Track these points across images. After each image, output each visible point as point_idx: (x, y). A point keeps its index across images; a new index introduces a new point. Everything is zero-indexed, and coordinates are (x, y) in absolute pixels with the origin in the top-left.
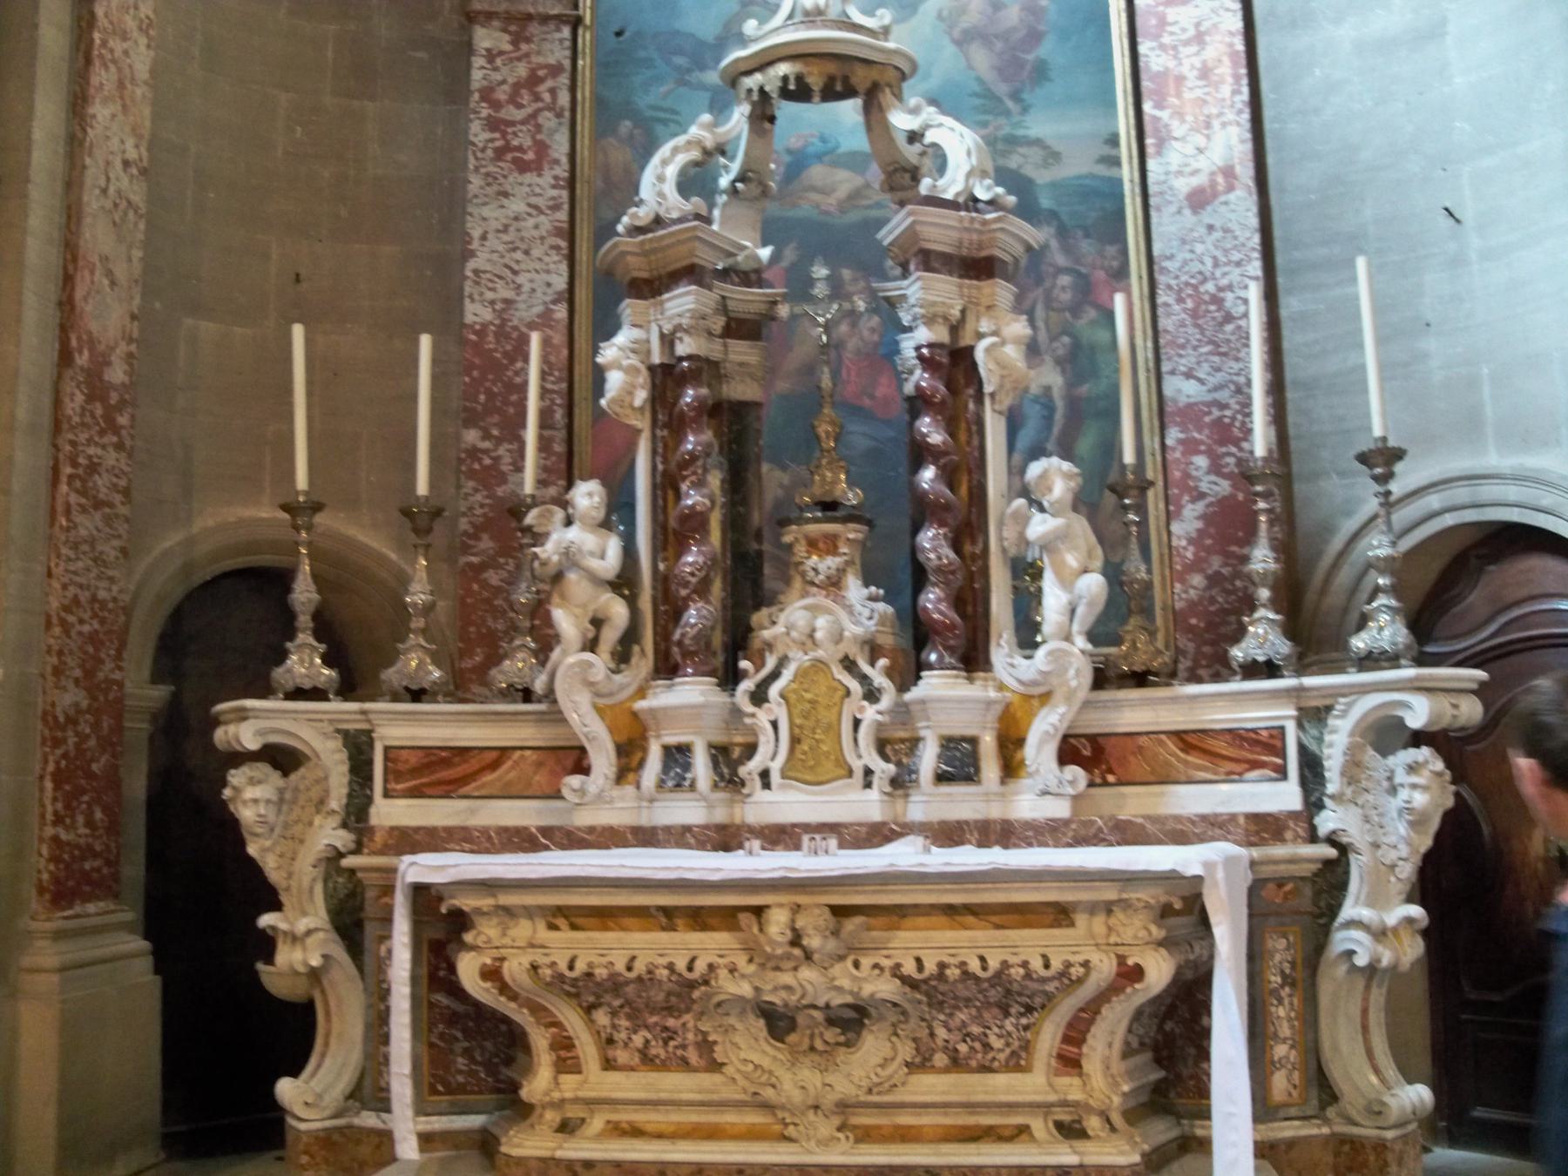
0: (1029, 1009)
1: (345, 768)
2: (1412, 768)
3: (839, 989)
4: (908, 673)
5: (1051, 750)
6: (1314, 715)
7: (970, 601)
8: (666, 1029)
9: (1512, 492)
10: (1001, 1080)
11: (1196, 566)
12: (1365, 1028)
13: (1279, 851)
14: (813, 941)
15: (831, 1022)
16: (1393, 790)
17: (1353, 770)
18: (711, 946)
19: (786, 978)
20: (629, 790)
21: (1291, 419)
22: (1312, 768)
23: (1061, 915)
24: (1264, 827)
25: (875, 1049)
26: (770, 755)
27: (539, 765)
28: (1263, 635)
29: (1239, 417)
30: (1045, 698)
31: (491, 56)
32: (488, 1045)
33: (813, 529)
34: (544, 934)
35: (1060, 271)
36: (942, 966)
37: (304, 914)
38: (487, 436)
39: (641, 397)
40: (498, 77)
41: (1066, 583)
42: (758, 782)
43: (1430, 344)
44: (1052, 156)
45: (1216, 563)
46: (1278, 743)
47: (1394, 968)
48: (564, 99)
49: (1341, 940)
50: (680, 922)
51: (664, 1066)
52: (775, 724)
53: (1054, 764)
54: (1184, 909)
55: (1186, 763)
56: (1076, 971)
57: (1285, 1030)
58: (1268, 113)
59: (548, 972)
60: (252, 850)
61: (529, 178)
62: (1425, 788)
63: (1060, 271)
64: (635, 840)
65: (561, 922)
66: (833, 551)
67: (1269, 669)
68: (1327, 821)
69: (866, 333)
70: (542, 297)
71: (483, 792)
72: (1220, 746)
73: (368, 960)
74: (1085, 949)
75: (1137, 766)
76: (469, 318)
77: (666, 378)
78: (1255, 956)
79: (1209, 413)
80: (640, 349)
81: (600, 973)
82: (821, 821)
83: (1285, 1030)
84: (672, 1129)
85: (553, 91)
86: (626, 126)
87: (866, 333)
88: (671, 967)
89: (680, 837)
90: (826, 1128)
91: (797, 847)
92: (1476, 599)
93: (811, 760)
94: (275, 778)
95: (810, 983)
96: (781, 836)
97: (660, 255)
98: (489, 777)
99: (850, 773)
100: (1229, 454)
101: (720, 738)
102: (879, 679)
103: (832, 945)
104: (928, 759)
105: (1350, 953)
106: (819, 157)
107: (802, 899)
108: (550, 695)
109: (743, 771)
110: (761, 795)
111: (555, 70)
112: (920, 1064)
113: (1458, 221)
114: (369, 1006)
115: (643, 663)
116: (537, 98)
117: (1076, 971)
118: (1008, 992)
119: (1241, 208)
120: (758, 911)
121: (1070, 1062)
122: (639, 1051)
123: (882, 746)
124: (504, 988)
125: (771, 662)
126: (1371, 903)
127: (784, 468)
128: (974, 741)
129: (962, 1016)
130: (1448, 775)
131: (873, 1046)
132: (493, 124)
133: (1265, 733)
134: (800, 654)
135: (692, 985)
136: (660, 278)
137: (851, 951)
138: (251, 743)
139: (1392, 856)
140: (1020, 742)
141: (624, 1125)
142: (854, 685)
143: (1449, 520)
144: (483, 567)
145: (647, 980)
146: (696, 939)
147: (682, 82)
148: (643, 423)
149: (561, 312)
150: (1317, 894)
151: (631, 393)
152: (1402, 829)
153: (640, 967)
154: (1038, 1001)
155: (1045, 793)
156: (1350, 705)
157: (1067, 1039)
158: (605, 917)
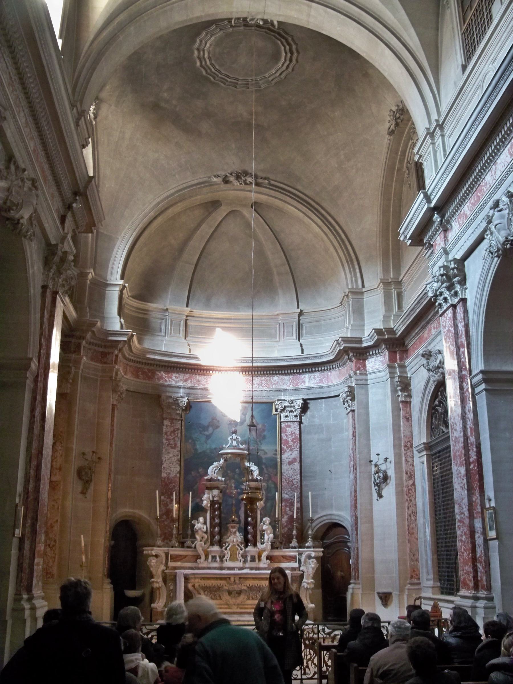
2: (312, 562)
4: (246, 546)
6: (300, 554)
7: (255, 537)
9: (337, 518)
11: (286, 526)
13: (295, 572)
14: (237, 582)
17: (305, 561)
18: (223, 582)
19: (233, 586)
21: (303, 502)
22: (300, 561)
24: (293, 569)
25: (242, 597)
26: (227, 557)
28: (294, 543)
30: (265, 551)
31: (167, 426)
33: (232, 525)
35: (266, 474)
38: (165, 497)
39: (209, 505)
40: (168, 430)
41: (268, 535)
43: (326, 492)
44: (266, 453)
45: (289, 526)
48: (179, 435)
49: (303, 584)
58: (302, 448)
60: (151, 569)
61: (173, 450)
63: (266, 474)
64: (208, 568)
66: (235, 528)
67: (295, 548)
68: (302, 568)
70: (175, 472)
72: (288, 558)
76: (162, 476)
77: (213, 503)
80: (209, 498)
82: (234, 566)
85: (178, 433)
86: (190, 441)
89: (215, 568)
90: (235, 607)
92: (331, 533)
93: (233, 558)
95: (236, 587)
102: (242, 547)
104: (249, 558)
108: (195, 547)
111: (178, 429)
112: (248, 599)
115: (208, 544)
116: (175, 434)
119: (297, 465)
120: (229, 578)
123: (242, 556)
124: (194, 588)
125: (227, 545)
129: (254, 592)
132: (167, 439)
135: (220, 588)
137: (241, 583)
142: (239, 548)
143: (327, 521)
144: (164, 521)
145: (214, 587)
147: (201, 433)
148: (209, 509)
149: (178, 475)
153: (213, 585)
158: (208, 578)
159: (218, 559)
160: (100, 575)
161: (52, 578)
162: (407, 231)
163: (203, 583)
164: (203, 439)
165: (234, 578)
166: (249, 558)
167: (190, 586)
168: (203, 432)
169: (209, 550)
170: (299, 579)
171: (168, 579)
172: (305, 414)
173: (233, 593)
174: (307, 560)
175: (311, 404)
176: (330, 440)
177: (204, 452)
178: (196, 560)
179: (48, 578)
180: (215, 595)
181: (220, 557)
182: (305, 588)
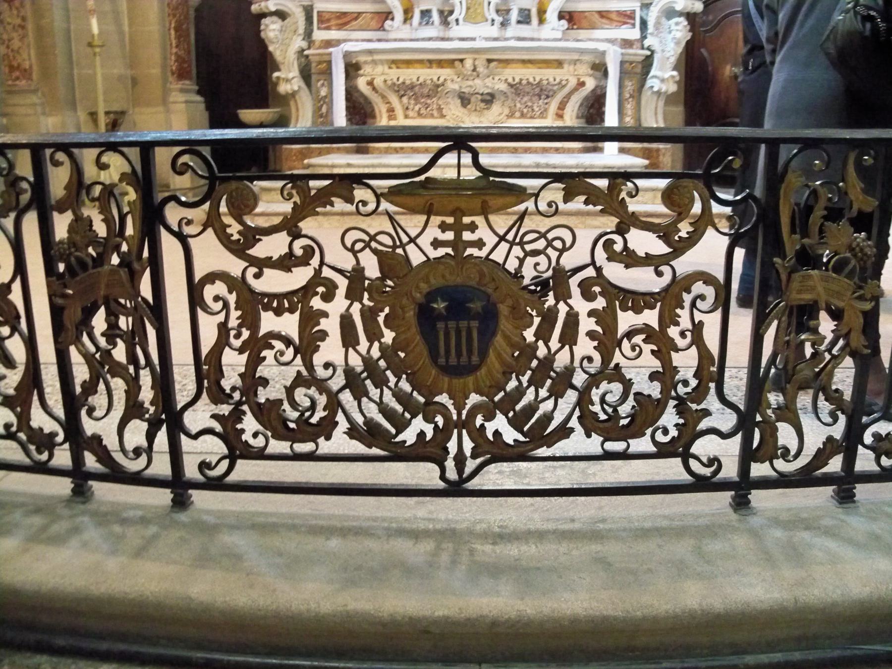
0: (548, 97)
1: (304, 18)
2: (677, 24)
3: (487, 87)
5: (556, 14)
12: (656, 114)
13: (631, 51)
14: (480, 69)
15: (482, 101)
16: (670, 32)
17: (658, 24)
18: (445, 73)
19: (470, 83)
20: (408, 26)
22: (644, 24)
23: (559, 64)
24: (627, 43)
27: (372, 19)
32: (357, 117)
36: (521, 80)
37: (290, 72)
42: (455, 23)
47: (666, 92)
49: (650, 82)
50: (434, 65)
51: (425, 117)
54: (600, 69)
56: (564, 83)
57: (629, 112)
62: (681, 31)
65: (393, 66)
68: (647, 43)
72: (614, 16)
73: (314, 89)
74: (567, 75)
75: (584, 23)
78: (621, 86)
81: (408, 82)
83: (629, 112)
88: (432, 80)
94: (280, 21)
95: (481, 85)
98: (354, 23)
99: (487, 20)
101: (441, 8)
103: (486, 71)
104: (514, 16)
105: (652, 87)
107: (476, 56)
109: (450, 19)
110: (455, 27)
112: (511, 116)
114: (314, 105)
117: (564, 83)
118: (541, 90)
120: (462, 61)
121: (560, 116)
124: (374, 89)
126: (661, 69)
128: (529, 10)
129: (525, 99)
130: (688, 27)
131: (496, 108)
135: (438, 86)
138: (273, 8)
139: (668, 55)
140: (545, 12)
150: (643, 67)
152: (672, 45)
154: (551, 93)
155: (553, 29)
157: (559, 108)
158: (408, 63)
159: (436, 17)
160: (156, 71)
161: (24, 78)
162: (403, 547)
163: (395, 74)
165: (475, 59)
166: (514, 16)
167: (361, 83)
170: (639, 69)
173: (473, 99)
174: (664, 20)
178: (382, 26)
179: (17, 78)
180: (427, 106)
181: (441, 12)
182: (654, 93)
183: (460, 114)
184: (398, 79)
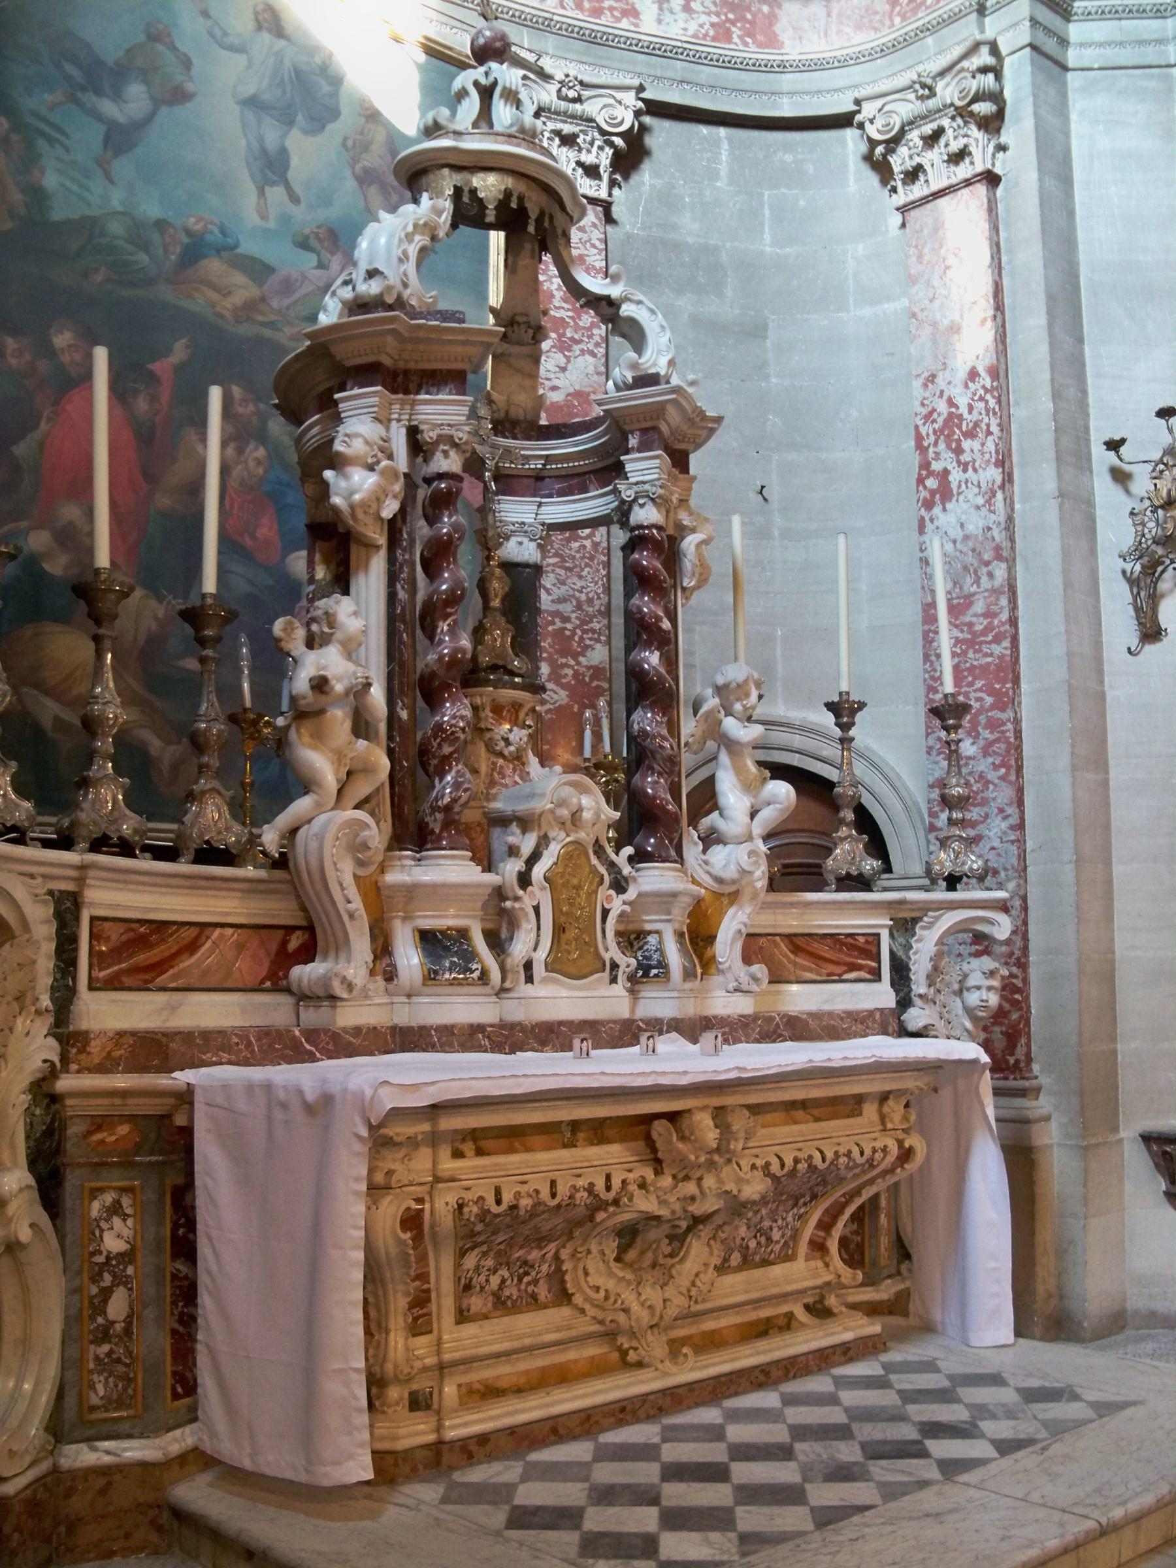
6: (905, 925)
8: (525, 1263)
10: (777, 1271)
22: (901, 973)
23: (852, 1105)
27: (240, 947)
29: (579, 632)
30: (734, 897)
34: (448, 1165)
46: (874, 950)
52: (537, 909)
53: (740, 962)
55: (795, 964)
59: (475, 1209)
69: (252, 464)
71: (180, 983)
72: (824, 950)
73: (72, 1225)
79: (553, 623)
84: (523, 1380)
87: (252, 464)
88: (590, 1189)
91: (567, 1047)
96: (551, 1036)
97: (421, 347)
98: (187, 962)
100: (567, 665)
106: (219, 250)
113: (765, 500)
114: (74, 1291)
120: (673, 1117)
122: (494, 1294)
127: (160, 599)
133: (862, 939)
134: (563, 834)
136: (406, 372)
140: (711, 939)
141: (477, 1386)
146: (595, 1153)
151: (379, 501)
156: (937, 918)
158: (514, 1137)
164: (87, 139)
168: (89, 99)
169: (393, 877)
171: (72, 1147)
172: (626, 177)
175: (664, 136)
176: (758, 331)
177: (89, 227)
183: (611, 1284)
184: (498, 1192)
